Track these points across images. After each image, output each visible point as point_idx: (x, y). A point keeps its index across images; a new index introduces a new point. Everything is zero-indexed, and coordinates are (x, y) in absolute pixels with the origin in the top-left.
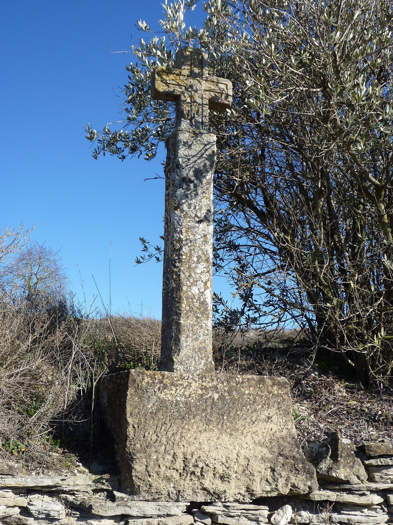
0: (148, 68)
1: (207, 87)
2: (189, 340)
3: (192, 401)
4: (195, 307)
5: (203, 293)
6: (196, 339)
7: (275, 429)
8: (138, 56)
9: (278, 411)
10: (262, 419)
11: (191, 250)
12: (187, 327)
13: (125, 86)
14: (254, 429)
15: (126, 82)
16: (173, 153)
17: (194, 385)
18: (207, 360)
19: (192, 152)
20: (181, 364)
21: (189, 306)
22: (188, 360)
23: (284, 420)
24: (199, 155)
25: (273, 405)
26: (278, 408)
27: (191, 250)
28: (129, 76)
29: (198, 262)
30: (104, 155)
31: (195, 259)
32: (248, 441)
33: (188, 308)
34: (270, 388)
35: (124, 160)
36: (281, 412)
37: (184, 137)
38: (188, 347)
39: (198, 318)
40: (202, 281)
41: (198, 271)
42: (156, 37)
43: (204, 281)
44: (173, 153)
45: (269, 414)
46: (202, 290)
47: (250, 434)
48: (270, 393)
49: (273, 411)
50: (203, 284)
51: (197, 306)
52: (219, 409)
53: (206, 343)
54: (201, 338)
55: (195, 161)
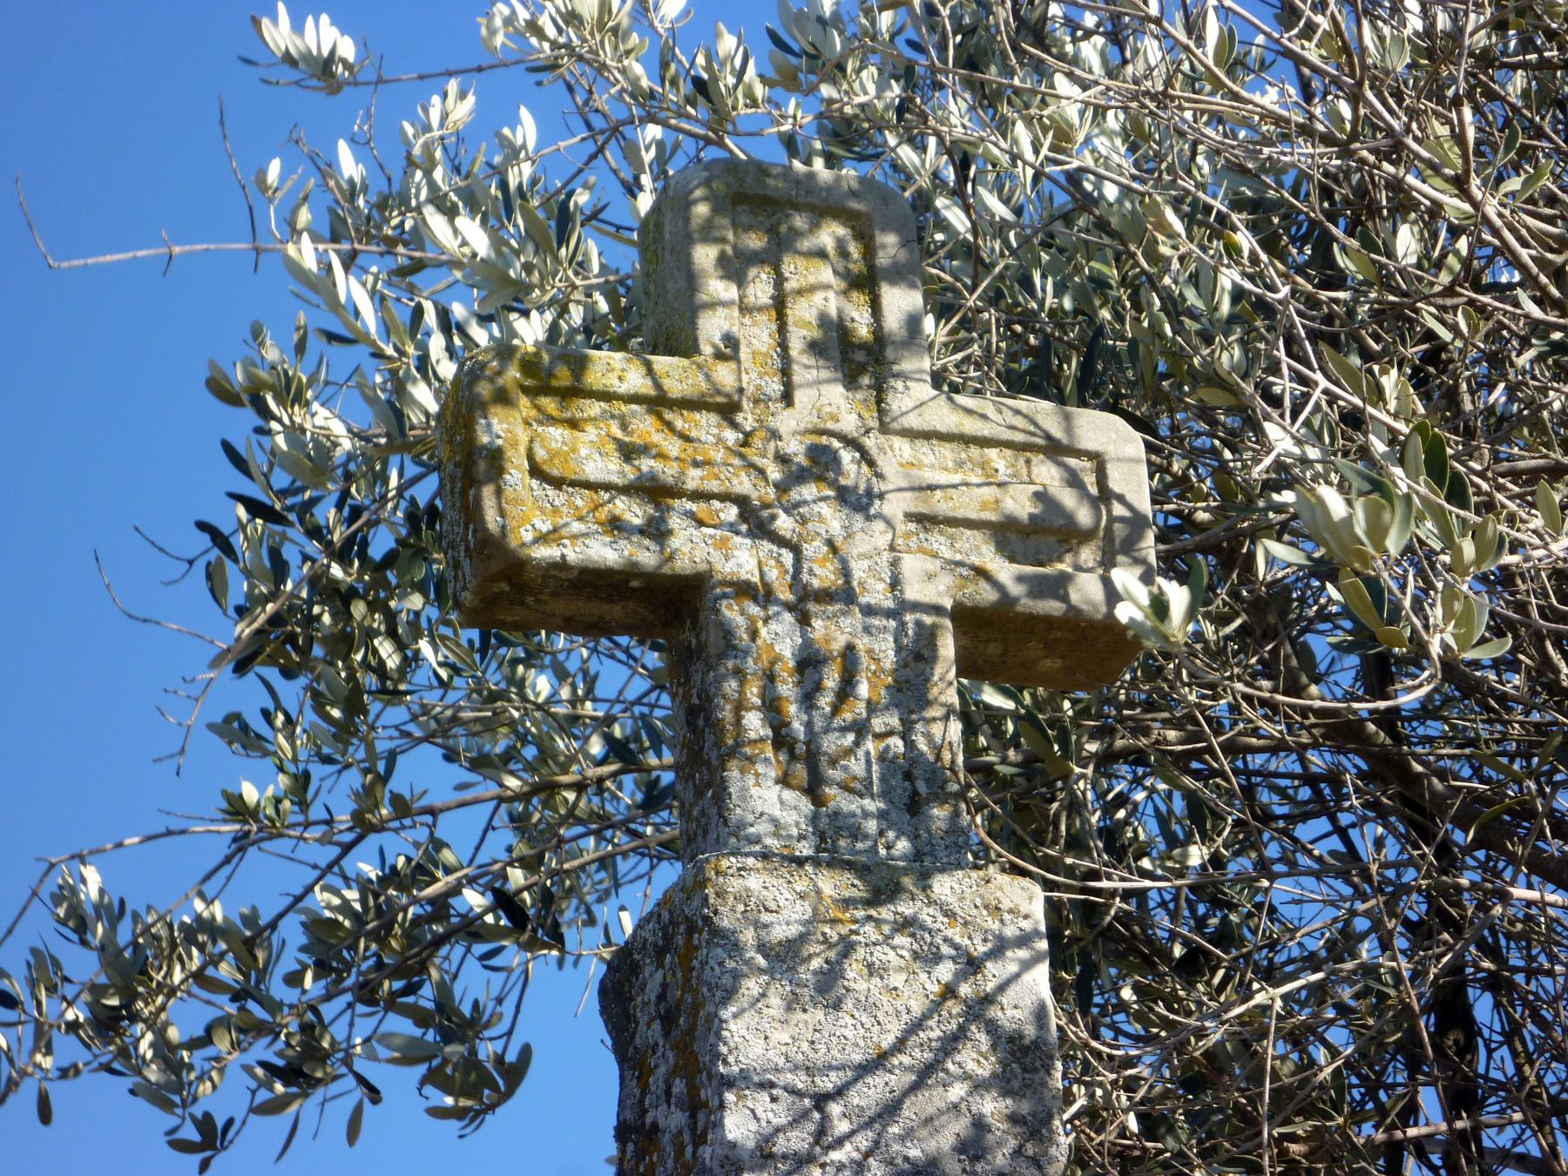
0: (379, 355)
1: (931, 494)
8: (296, 269)
13: (203, 526)
15: (215, 495)
16: (679, 1086)
19: (850, 1034)
24: (914, 1056)
28: (228, 448)
30: (45, 1114)
35: (220, 1161)
37: (767, 897)
42: (453, 86)
44: (679, 1086)
55: (891, 1110)
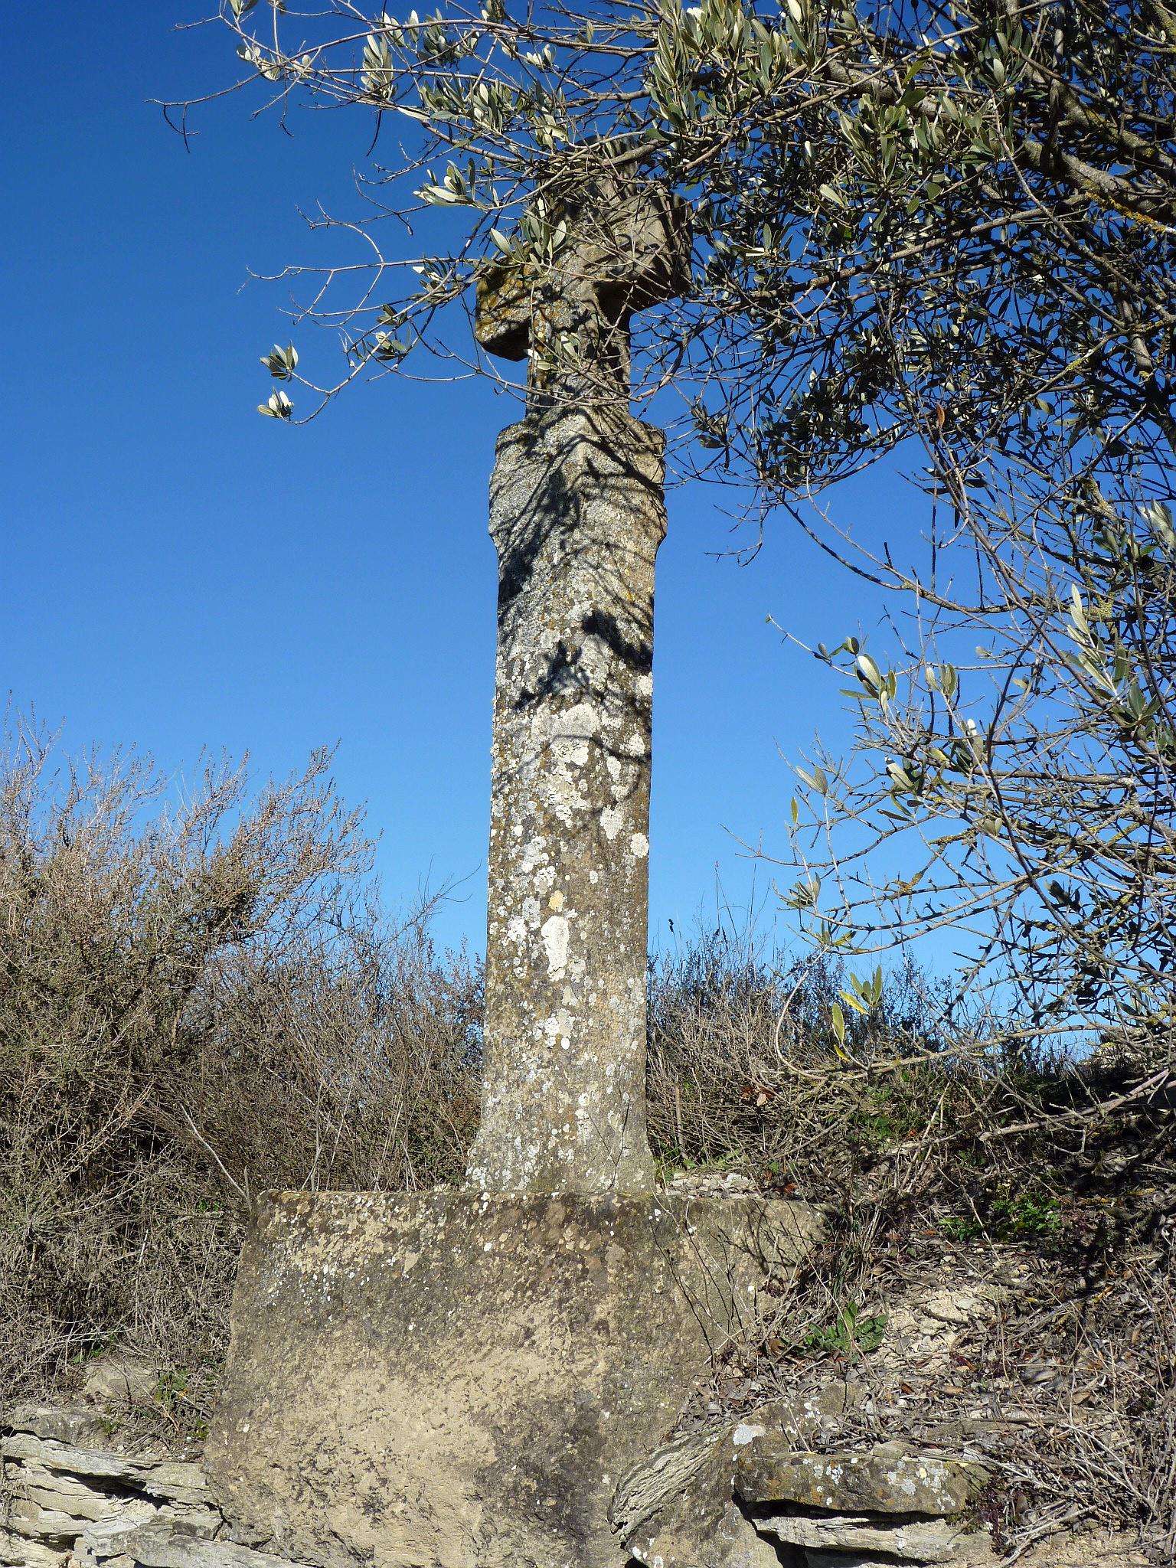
2: (502, 1086)
3: (352, 1275)
4: (520, 981)
5: (537, 933)
6: (519, 1082)
7: (538, 1370)
9: (555, 1311)
10: (504, 1334)
11: (510, 805)
12: (497, 1046)
14: (477, 1368)
17: (373, 1228)
18: (545, 1146)
20: (481, 1164)
21: (503, 982)
22: (499, 1148)
23: (568, 1342)
25: (547, 1290)
26: (561, 1301)
27: (510, 805)
29: (526, 838)
31: (518, 830)
32: (451, 1405)
33: (501, 988)
34: (553, 1234)
36: (564, 1314)
38: (499, 1108)
39: (524, 1013)
40: (536, 896)
41: (527, 867)
43: (543, 893)
45: (532, 1320)
46: (534, 926)
47: (461, 1382)
48: (550, 1247)
49: (540, 1313)
50: (538, 905)
51: (523, 976)
52: (404, 1301)
53: (545, 1090)
54: (532, 1077)
